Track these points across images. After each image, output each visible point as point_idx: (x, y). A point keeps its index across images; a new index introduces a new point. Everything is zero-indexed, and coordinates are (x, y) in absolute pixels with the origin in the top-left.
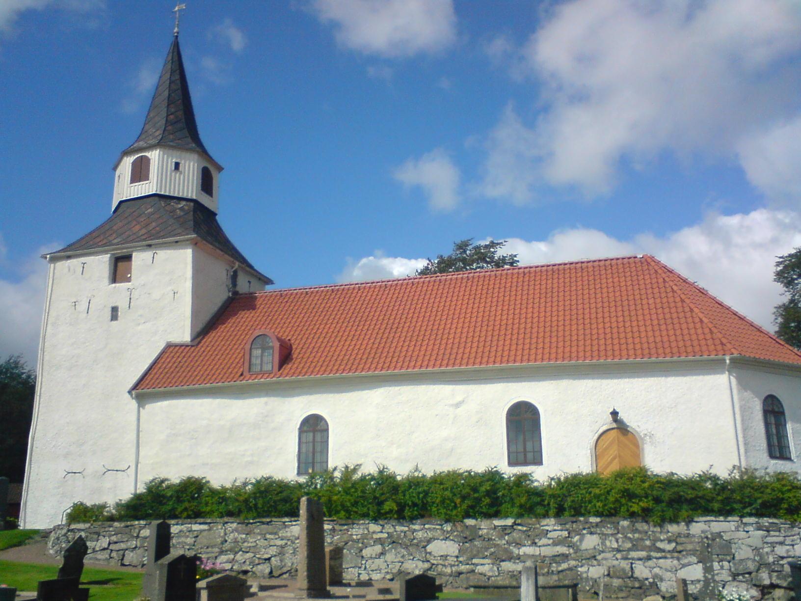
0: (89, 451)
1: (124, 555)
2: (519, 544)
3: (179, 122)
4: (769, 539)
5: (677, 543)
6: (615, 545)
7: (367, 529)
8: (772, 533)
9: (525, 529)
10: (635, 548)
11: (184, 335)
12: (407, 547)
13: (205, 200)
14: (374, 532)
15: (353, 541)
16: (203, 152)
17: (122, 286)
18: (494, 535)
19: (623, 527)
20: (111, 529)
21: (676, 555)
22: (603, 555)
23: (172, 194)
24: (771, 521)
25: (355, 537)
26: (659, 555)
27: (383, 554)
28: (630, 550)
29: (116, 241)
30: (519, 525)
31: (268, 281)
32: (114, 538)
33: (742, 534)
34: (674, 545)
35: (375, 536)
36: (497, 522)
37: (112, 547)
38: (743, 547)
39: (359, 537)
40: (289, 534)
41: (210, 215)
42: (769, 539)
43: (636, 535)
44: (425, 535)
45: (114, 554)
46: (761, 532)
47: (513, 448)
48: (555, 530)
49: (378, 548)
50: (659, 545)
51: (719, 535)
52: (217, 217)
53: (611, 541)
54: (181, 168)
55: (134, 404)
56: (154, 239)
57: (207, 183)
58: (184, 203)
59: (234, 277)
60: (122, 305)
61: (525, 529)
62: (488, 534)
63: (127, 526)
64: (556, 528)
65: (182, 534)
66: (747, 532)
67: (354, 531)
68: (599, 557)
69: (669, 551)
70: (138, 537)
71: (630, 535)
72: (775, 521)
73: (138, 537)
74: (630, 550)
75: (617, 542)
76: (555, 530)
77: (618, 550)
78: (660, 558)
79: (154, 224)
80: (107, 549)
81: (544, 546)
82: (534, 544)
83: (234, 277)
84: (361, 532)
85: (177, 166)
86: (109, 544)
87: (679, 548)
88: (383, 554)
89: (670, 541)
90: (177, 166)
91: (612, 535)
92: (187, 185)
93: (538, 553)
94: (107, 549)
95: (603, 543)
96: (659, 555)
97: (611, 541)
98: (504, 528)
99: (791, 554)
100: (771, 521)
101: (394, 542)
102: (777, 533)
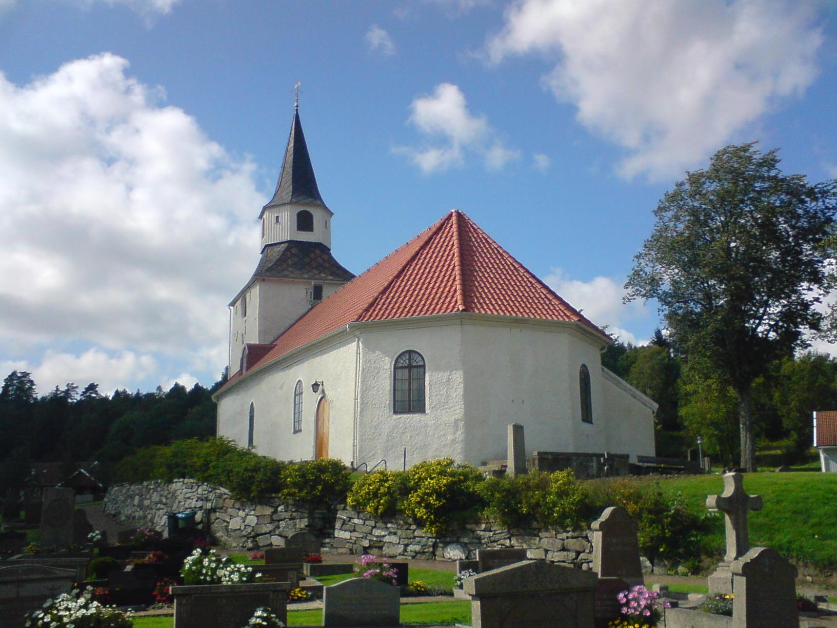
13: (304, 237)
57: (305, 222)
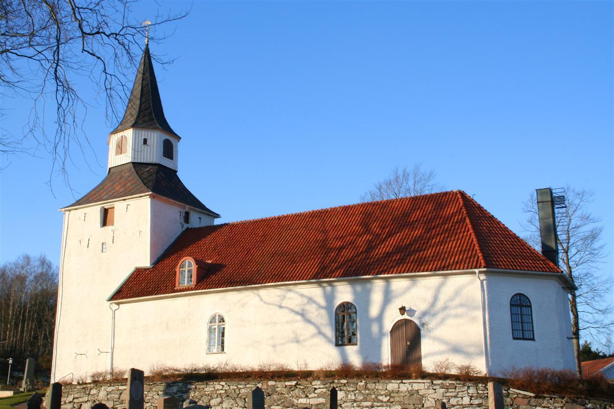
0: (94, 339)
1: (81, 405)
2: (298, 397)
3: (148, 111)
4: (448, 394)
5: (390, 397)
6: (353, 398)
7: (214, 387)
8: (450, 390)
9: (302, 387)
10: (365, 400)
11: (146, 263)
12: (235, 399)
13: (166, 162)
14: (218, 390)
15: (206, 395)
16: (165, 127)
17: (108, 228)
18: (285, 391)
19: (360, 386)
20: (75, 390)
21: (389, 404)
22: (345, 404)
23: (142, 162)
24: (450, 382)
25: (207, 393)
26: (379, 404)
27: (221, 403)
28: (361, 401)
29: (105, 197)
30: (300, 385)
31: (217, 216)
32: (76, 396)
33: (431, 391)
34: (388, 398)
35: (218, 392)
36: (287, 383)
37: (76, 401)
38: (430, 399)
39: (209, 392)
40: (171, 391)
41: (172, 174)
42: (448, 394)
43: (367, 392)
44: (246, 391)
45: (75, 405)
46: (443, 389)
47: (53, 327)
48: (320, 388)
49: (219, 400)
50: (380, 398)
51: (417, 391)
52: (177, 173)
53: (351, 395)
54: (148, 142)
55: (108, 307)
56: (127, 192)
58: (150, 167)
59: (187, 218)
60: (109, 241)
61: (302, 387)
62: (281, 390)
63: (84, 388)
64: (320, 387)
65: (113, 392)
66: (435, 389)
67: (207, 389)
68: (343, 406)
69: (385, 402)
70: (89, 394)
71: (363, 391)
72: (454, 382)
73: (89, 394)
74: (361, 401)
75: (355, 395)
76: (320, 388)
77: (355, 401)
78: (379, 406)
79: (129, 184)
80: (72, 402)
81: (312, 398)
82: (307, 396)
83: (187, 218)
84: (211, 389)
85: (145, 141)
86: (74, 399)
87: (392, 400)
88: (221, 403)
89: (386, 396)
90: (145, 141)
91: (353, 391)
92: (153, 155)
93: (308, 403)
94: (72, 402)
95: (347, 396)
96: (379, 404)
97: (351, 395)
98: (291, 387)
99: (460, 403)
100: (450, 382)
101: (228, 396)
102: (453, 390)
